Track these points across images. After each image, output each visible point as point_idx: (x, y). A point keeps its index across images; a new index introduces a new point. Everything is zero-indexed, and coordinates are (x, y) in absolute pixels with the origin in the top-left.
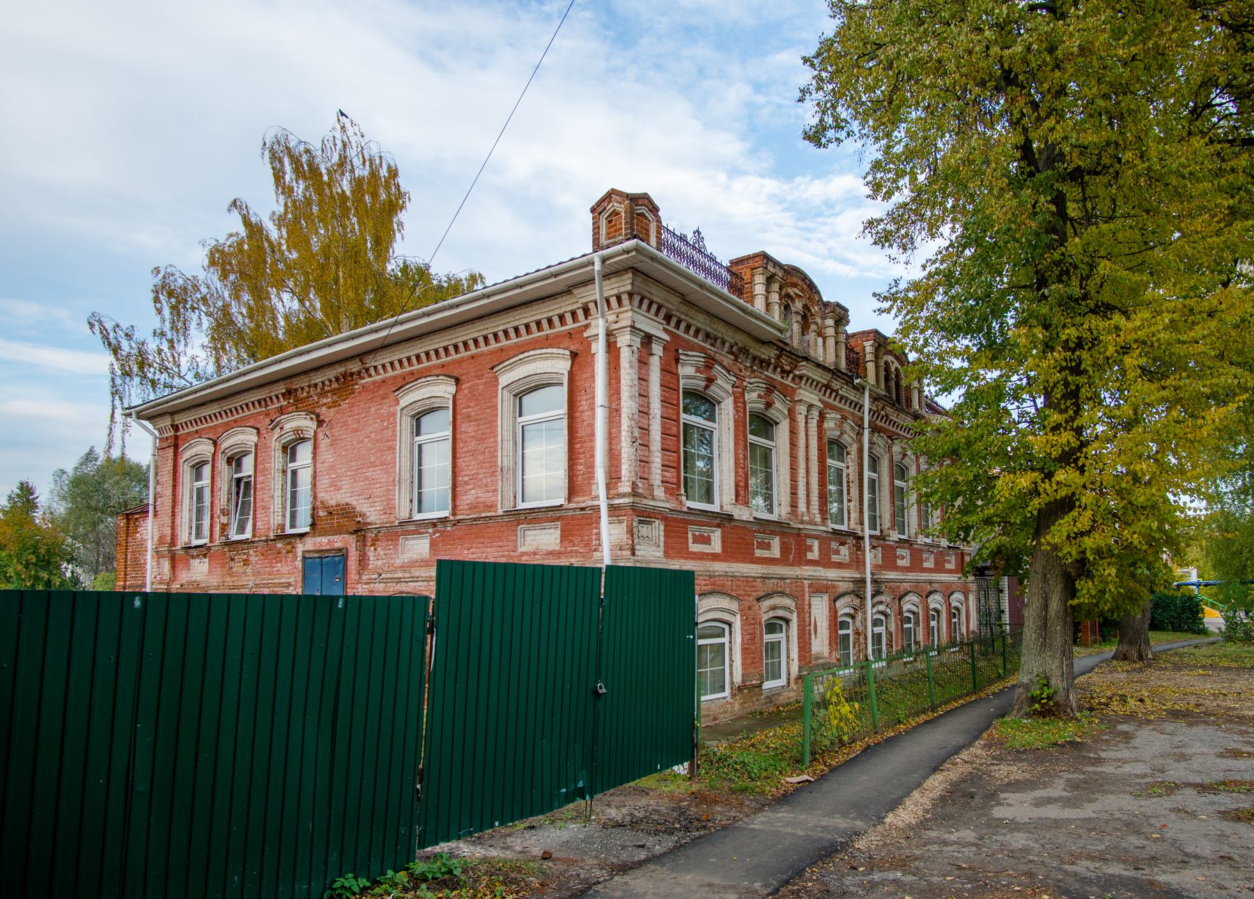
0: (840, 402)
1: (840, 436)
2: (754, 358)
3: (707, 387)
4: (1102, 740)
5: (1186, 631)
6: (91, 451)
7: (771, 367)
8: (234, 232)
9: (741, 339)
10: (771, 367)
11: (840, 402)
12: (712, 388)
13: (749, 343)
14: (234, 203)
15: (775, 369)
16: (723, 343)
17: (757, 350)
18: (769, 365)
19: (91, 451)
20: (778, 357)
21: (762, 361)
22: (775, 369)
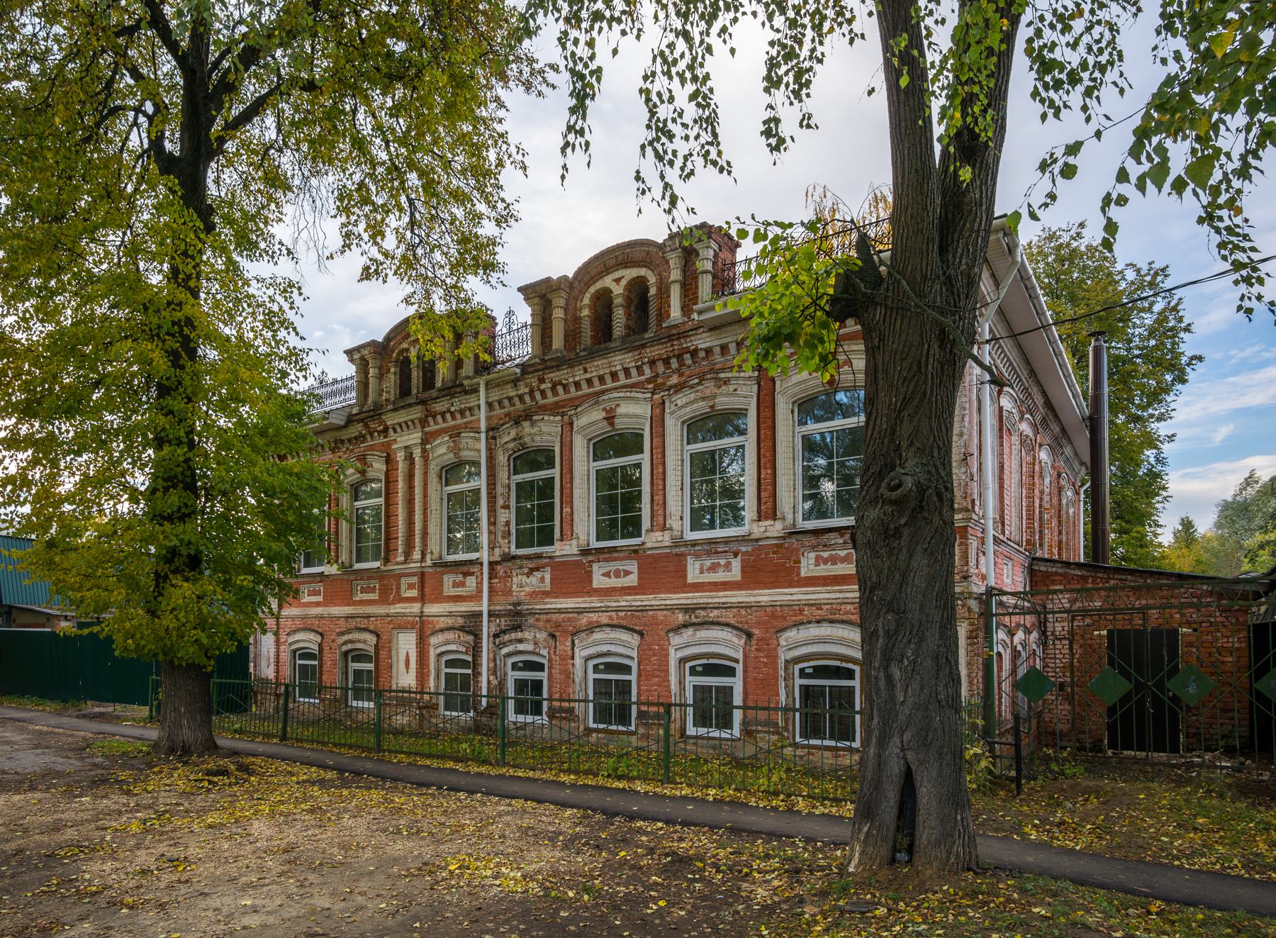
0: (444, 420)
1: (610, 419)
2: (349, 440)
3: (612, 424)
4: (432, 151)
5: (1147, 116)
6: (711, 54)
7: (368, 437)
8: (720, 139)
9: (331, 436)
10: (368, 437)
11: (444, 420)
12: (617, 421)
13: (337, 434)
14: (775, 149)
15: (372, 435)
16: (323, 446)
17: (345, 435)
18: (363, 436)
19: (711, 54)
20: (366, 426)
21: (356, 438)
22: (372, 435)
